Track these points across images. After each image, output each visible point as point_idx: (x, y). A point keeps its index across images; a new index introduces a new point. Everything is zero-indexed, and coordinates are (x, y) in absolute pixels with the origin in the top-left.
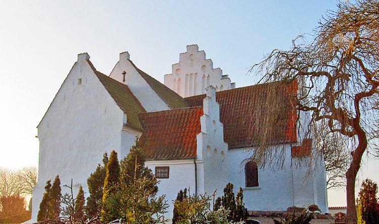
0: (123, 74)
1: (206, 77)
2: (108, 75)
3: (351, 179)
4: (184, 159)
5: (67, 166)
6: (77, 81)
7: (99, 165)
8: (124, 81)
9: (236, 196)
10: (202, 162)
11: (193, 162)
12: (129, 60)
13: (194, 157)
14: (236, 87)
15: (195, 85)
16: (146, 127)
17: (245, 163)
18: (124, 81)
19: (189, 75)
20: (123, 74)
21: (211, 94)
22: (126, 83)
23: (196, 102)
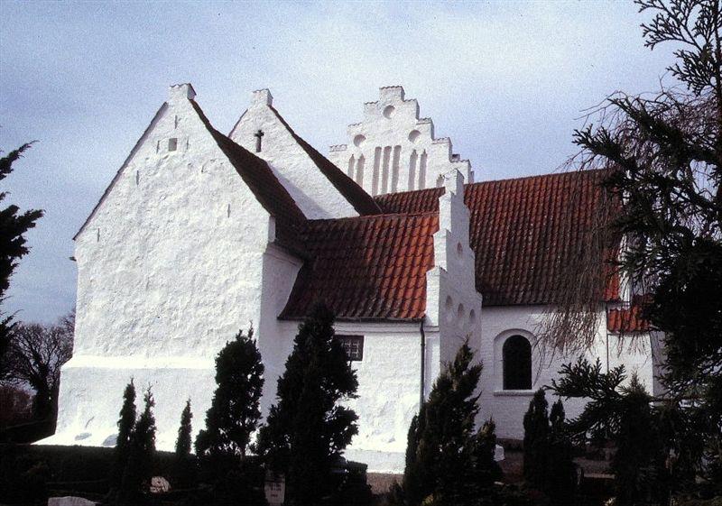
0: (256, 135)
1: (419, 156)
2: (227, 135)
3: (102, 347)
4: (397, 322)
5: (140, 323)
6: (165, 144)
7: (241, 331)
8: (259, 150)
9: (549, 409)
10: (437, 329)
11: (418, 329)
12: (270, 107)
13: (420, 321)
14: (426, 188)
15: (396, 170)
16: (311, 250)
17: (503, 340)
18: (259, 150)
19: (393, 149)
20: (256, 135)
21: (451, 187)
22: (260, 155)
23: (425, 201)
